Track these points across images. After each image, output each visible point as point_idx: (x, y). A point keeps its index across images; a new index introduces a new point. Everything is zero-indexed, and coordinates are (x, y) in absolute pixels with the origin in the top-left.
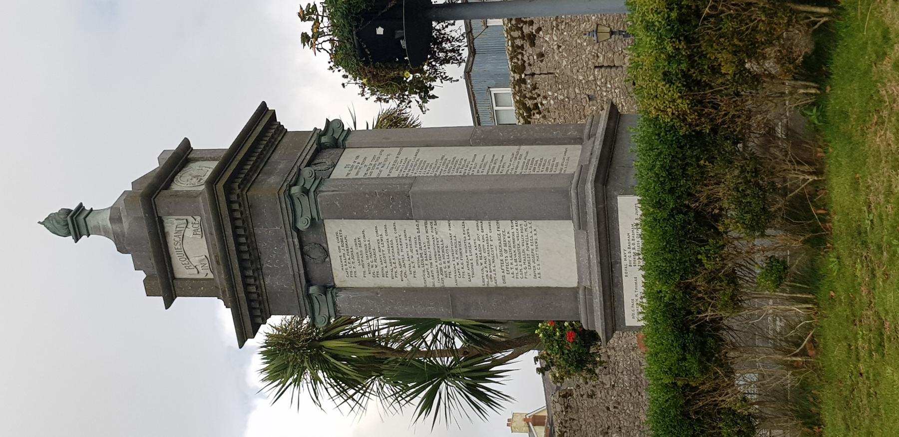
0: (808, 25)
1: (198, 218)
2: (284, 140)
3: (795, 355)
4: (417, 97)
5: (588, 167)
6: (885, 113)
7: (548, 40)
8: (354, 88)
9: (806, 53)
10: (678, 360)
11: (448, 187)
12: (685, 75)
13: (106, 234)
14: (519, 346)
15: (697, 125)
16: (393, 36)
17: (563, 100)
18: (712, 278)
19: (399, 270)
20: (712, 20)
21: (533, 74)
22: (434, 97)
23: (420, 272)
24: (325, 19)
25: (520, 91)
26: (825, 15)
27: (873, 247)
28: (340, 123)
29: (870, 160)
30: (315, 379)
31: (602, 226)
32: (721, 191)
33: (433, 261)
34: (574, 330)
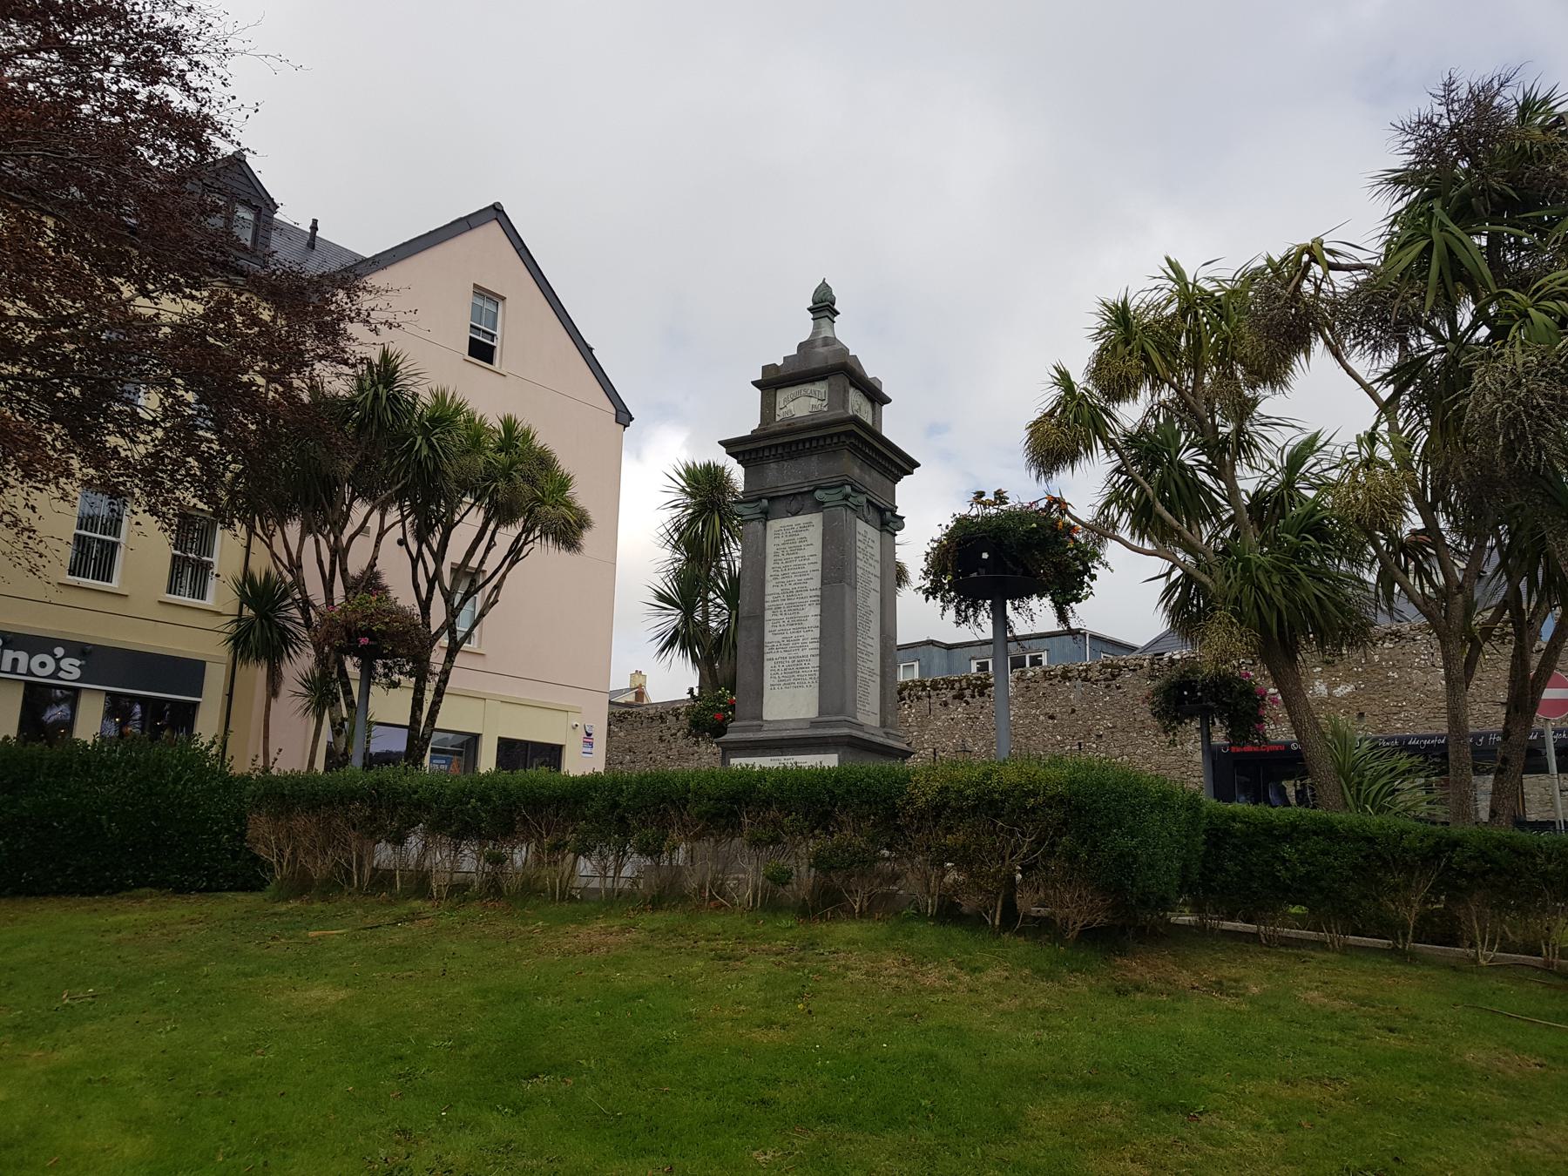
0: (985, 907)
1: (825, 409)
2: (888, 482)
3: (710, 891)
4: (928, 585)
5: (863, 731)
6: (912, 967)
7: (959, 711)
8: (938, 534)
9: (962, 906)
10: (709, 795)
11: (848, 613)
12: (946, 805)
13: (813, 334)
14: (709, 679)
15: (903, 814)
16: (982, 567)
17: (907, 721)
18: (776, 823)
19: (780, 573)
20: (991, 828)
21: (930, 697)
22: (927, 599)
23: (778, 590)
24: (996, 511)
25: (916, 686)
26: (993, 921)
27: (801, 954)
28: (901, 527)
29: (873, 954)
30: (687, 507)
31: (812, 741)
32: (848, 832)
33: (787, 602)
34: (724, 719)
